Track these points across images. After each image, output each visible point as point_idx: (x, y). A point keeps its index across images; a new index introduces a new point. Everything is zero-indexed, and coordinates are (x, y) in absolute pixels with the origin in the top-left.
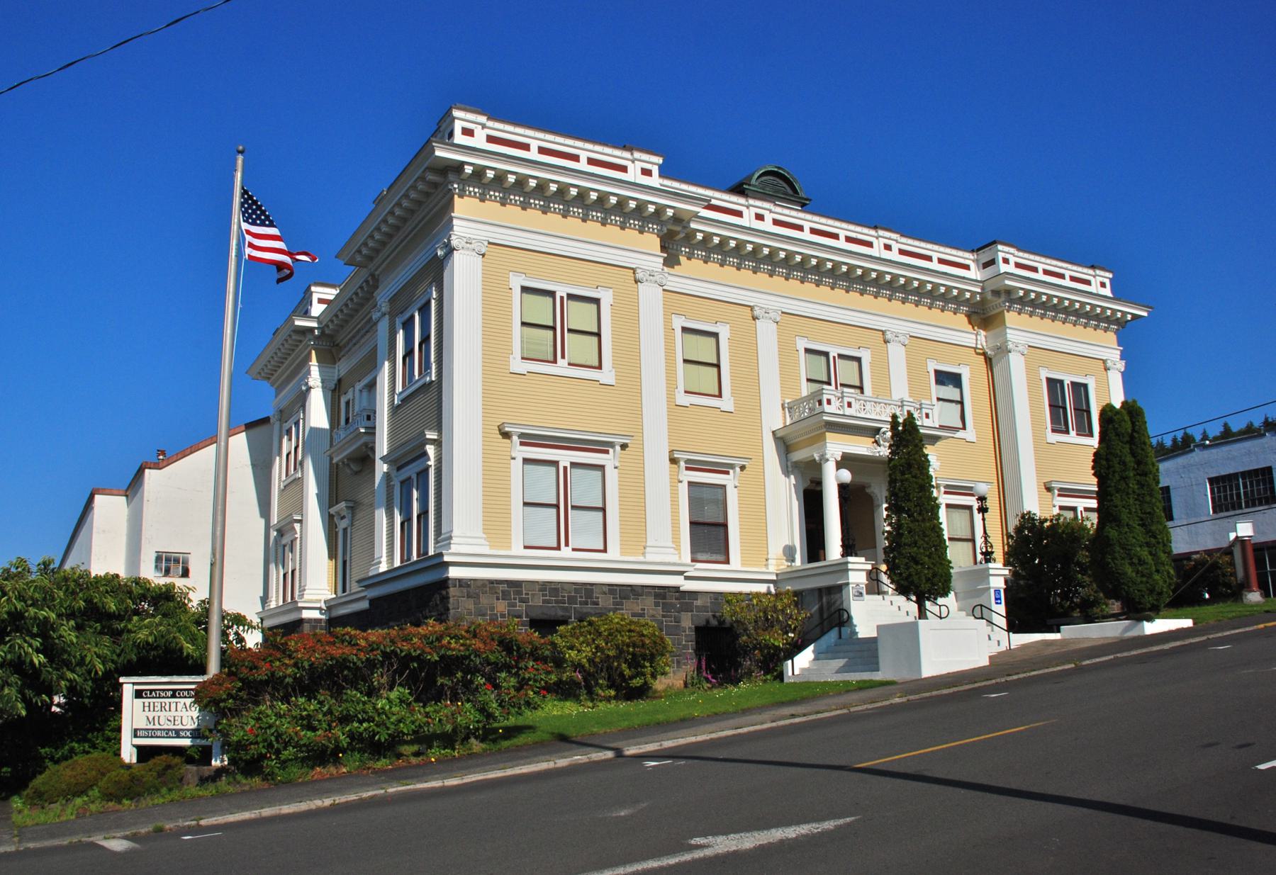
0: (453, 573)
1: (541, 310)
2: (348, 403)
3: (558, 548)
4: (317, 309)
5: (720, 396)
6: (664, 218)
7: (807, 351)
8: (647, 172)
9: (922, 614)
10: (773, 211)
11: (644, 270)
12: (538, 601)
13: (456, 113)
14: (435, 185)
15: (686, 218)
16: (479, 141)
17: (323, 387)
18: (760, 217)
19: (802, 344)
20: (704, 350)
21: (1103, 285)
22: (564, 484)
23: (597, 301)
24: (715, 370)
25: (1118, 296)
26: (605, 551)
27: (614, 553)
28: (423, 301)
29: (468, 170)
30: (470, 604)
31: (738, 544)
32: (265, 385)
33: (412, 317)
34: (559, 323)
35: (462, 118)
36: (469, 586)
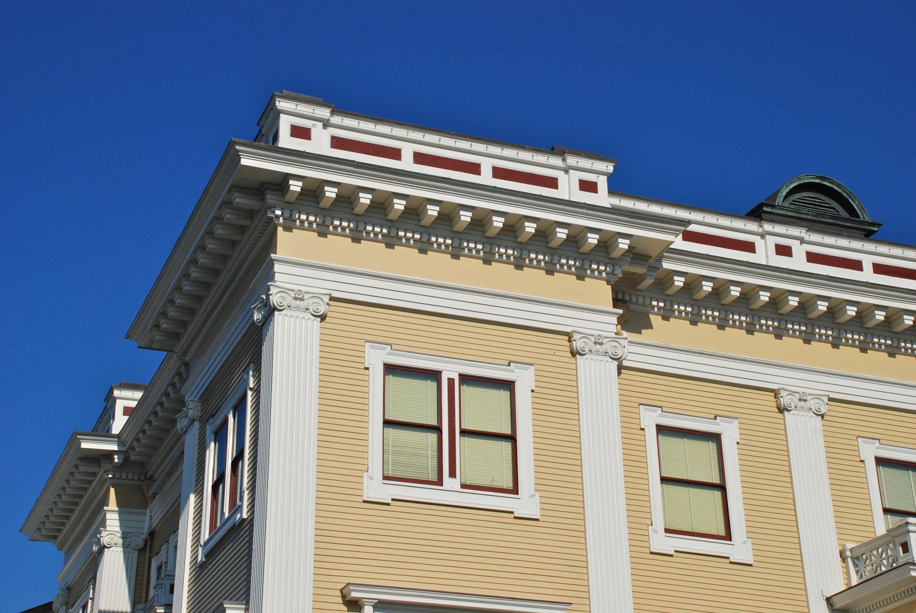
1: (417, 400)
2: (159, 569)
4: (119, 423)
5: (728, 537)
6: (616, 254)
7: (881, 462)
8: (588, 186)
10: (804, 242)
11: (585, 336)
13: (281, 104)
14: (251, 214)
15: (654, 254)
16: (319, 143)
17: (125, 546)
18: (783, 251)
20: (695, 461)
23: (716, 438)
24: (718, 494)
28: (238, 395)
29: (295, 186)
32: (50, 547)
33: (226, 421)
34: (446, 421)
35: (290, 112)
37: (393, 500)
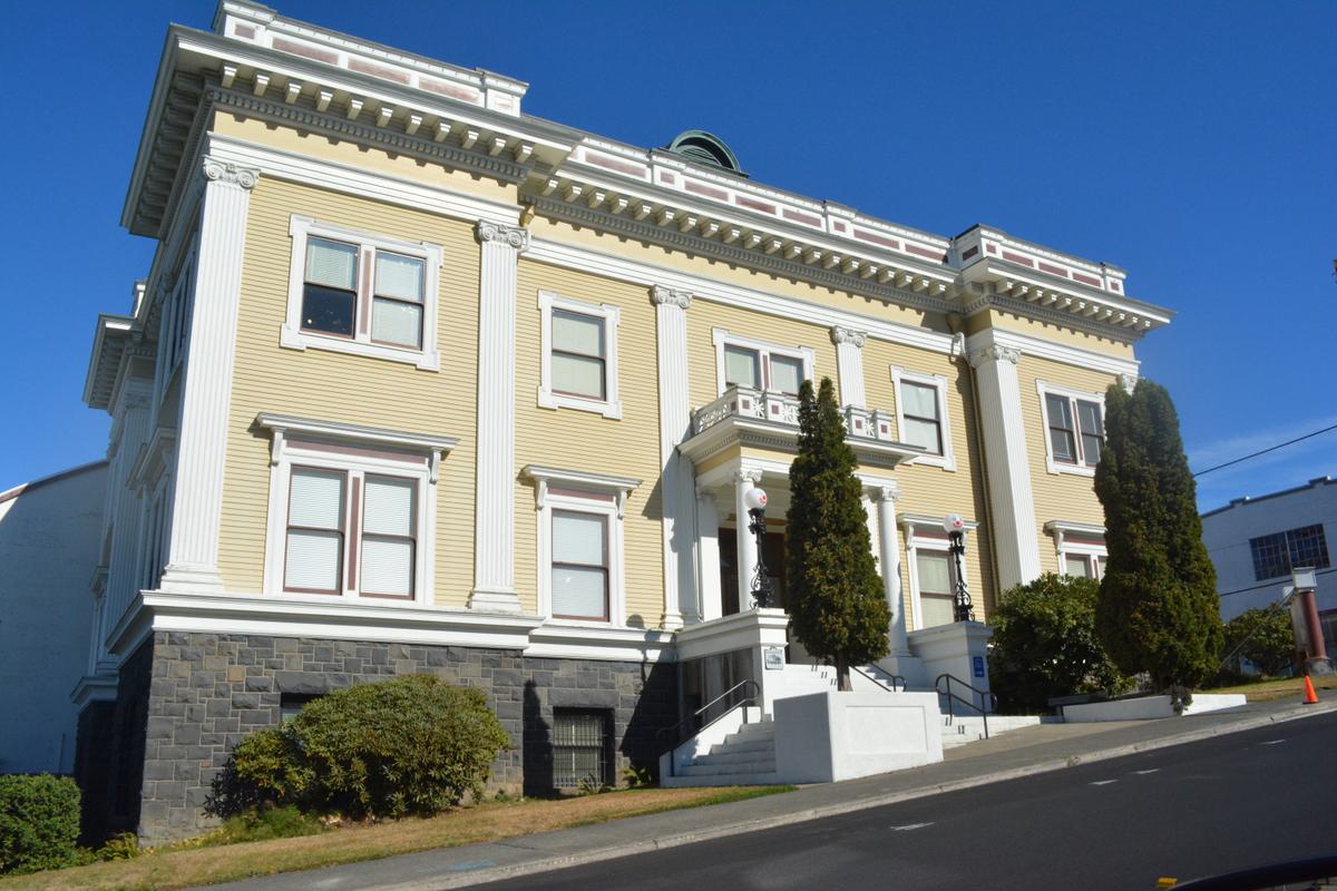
0: (160, 622)
3: (339, 591)
9: (842, 684)
11: (491, 224)
12: (297, 664)
13: (228, 6)
19: (720, 339)
20: (583, 338)
21: (1115, 286)
22: (348, 503)
25: (1134, 293)
26: (413, 596)
27: (426, 598)
30: (185, 670)
31: (622, 594)
36: (185, 643)
37: (308, 348)
